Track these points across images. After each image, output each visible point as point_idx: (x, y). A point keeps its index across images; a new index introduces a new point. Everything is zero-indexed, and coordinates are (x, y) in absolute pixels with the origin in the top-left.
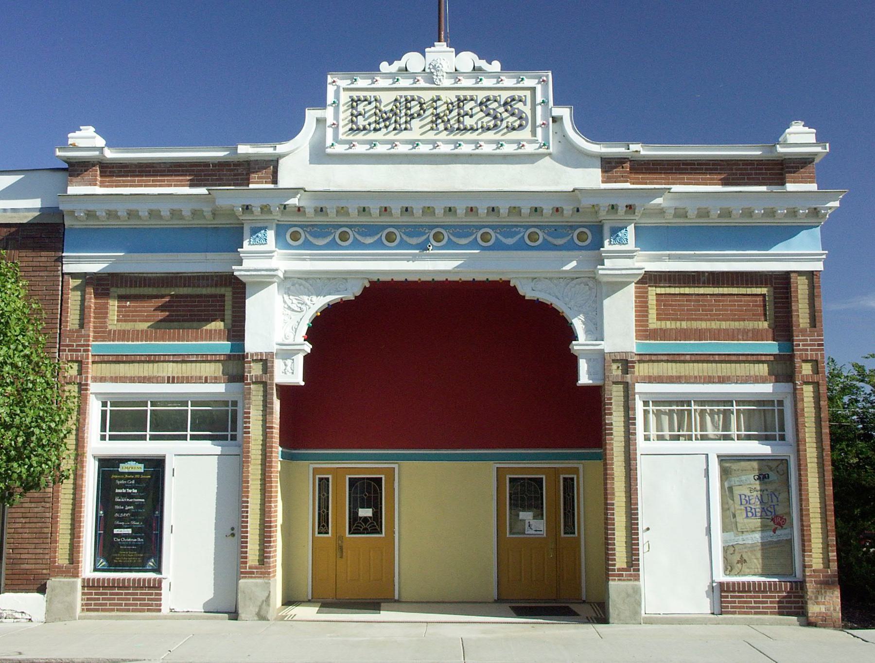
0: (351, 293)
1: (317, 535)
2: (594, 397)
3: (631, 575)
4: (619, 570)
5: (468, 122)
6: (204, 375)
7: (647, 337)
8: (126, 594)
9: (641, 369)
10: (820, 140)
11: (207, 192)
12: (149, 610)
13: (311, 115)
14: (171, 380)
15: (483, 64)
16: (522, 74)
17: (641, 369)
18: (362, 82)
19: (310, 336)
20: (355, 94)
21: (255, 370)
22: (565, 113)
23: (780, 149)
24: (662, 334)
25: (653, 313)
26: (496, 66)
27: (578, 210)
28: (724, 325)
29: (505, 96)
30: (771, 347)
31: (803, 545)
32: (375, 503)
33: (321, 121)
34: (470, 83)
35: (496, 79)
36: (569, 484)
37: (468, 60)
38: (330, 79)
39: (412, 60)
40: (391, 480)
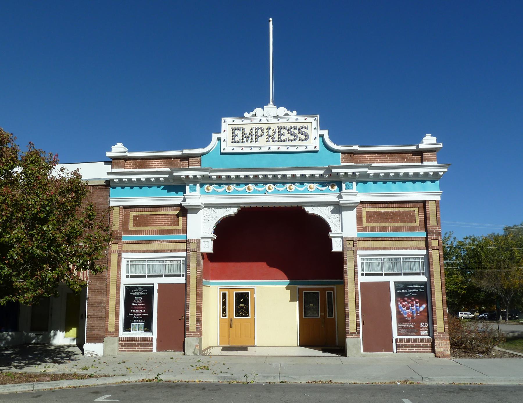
0: (233, 211)
1: (221, 317)
2: (340, 255)
3: (356, 335)
4: (351, 333)
5: (282, 138)
6: (170, 249)
7: (361, 230)
8: (131, 344)
9: (360, 244)
10: (438, 141)
11: (170, 170)
12: (147, 351)
13: (215, 136)
14: (156, 251)
15: (289, 112)
16: (306, 116)
17: (360, 244)
18: (238, 121)
19: (216, 232)
20: (234, 126)
21: (193, 246)
22: (325, 133)
23: (421, 146)
24: (367, 229)
25: (364, 220)
26: (295, 113)
27: (331, 175)
28: (396, 225)
29: (298, 126)
30: (422, 234)
31: (433, 322)
32: (247, 303)
33: (219, 139)
34: (285, 120)
35: (294, 119)
36: (330, 294)
37: (282, 110)
38: (223, 120)
39: (258, 111)
40: (253, 293)
